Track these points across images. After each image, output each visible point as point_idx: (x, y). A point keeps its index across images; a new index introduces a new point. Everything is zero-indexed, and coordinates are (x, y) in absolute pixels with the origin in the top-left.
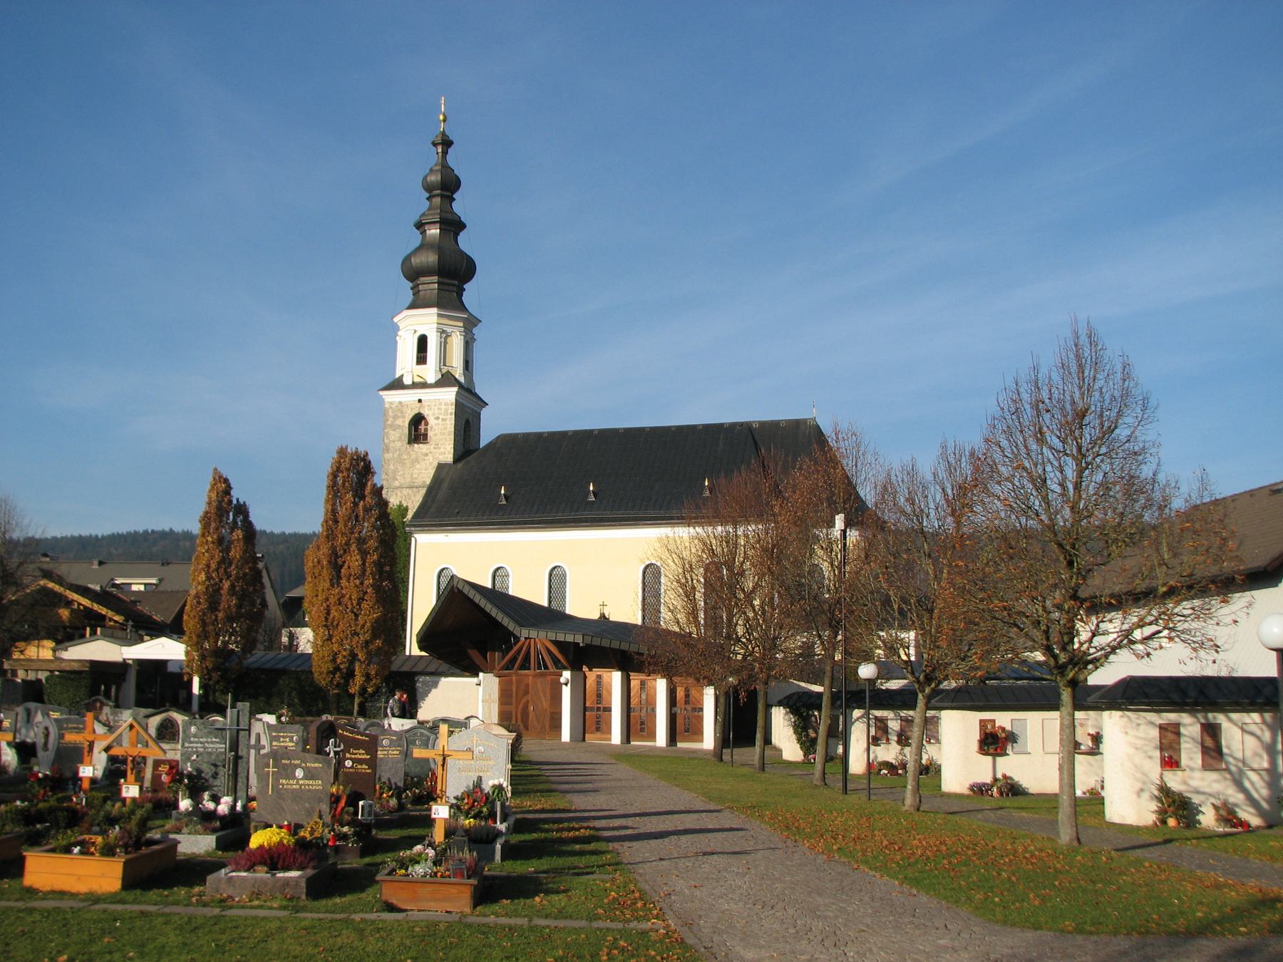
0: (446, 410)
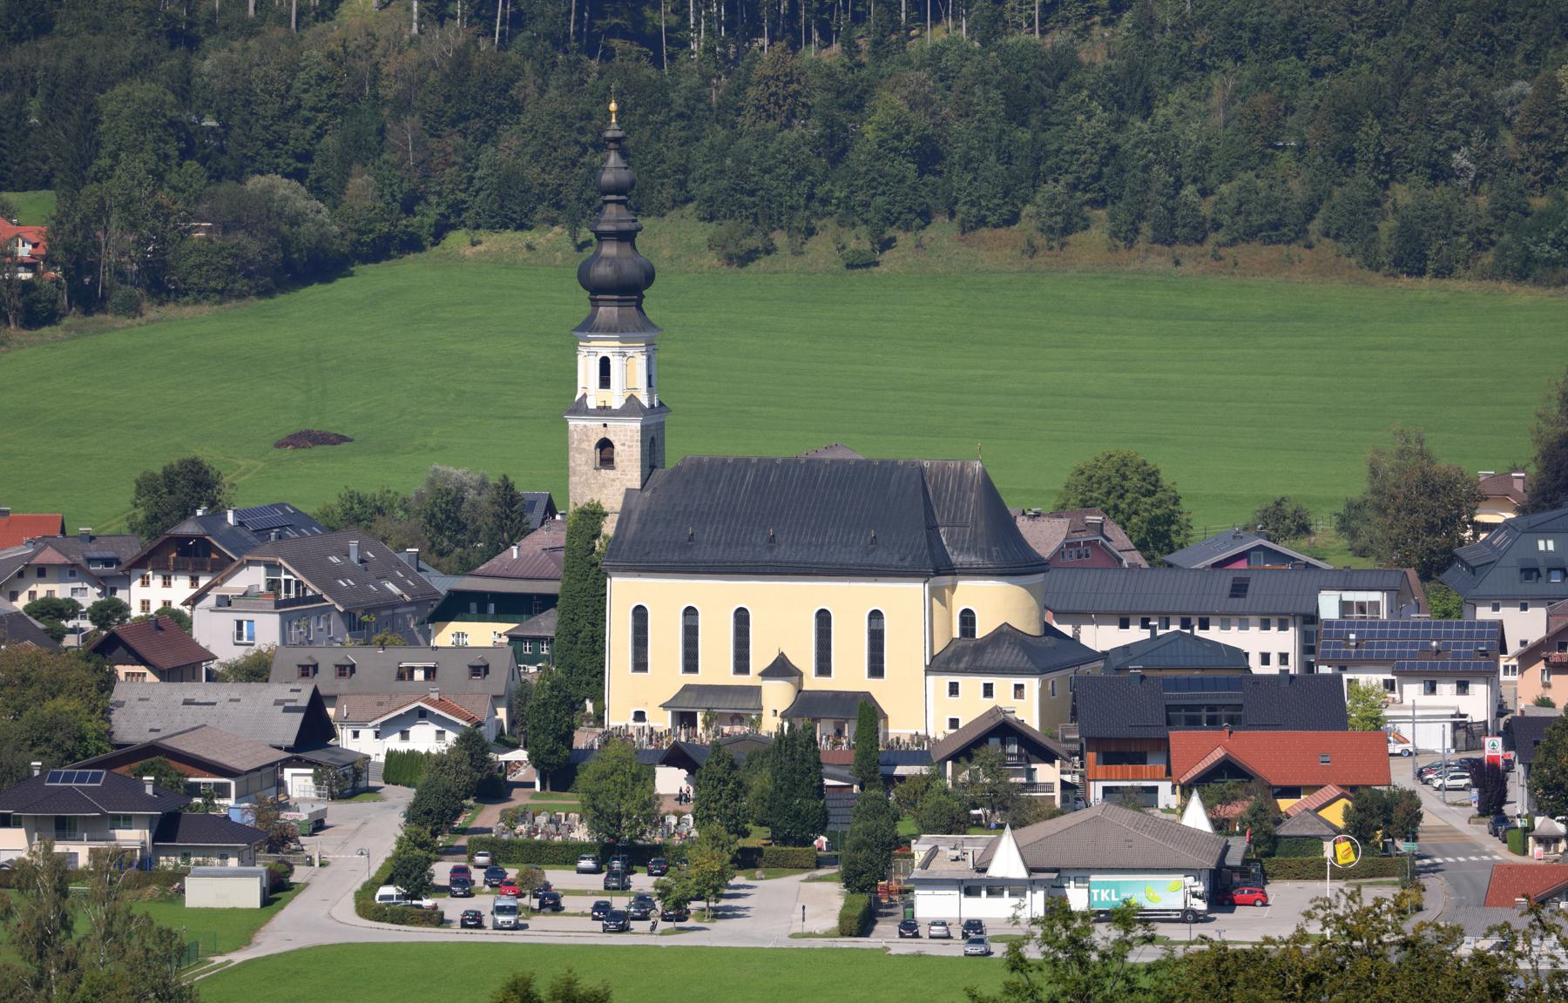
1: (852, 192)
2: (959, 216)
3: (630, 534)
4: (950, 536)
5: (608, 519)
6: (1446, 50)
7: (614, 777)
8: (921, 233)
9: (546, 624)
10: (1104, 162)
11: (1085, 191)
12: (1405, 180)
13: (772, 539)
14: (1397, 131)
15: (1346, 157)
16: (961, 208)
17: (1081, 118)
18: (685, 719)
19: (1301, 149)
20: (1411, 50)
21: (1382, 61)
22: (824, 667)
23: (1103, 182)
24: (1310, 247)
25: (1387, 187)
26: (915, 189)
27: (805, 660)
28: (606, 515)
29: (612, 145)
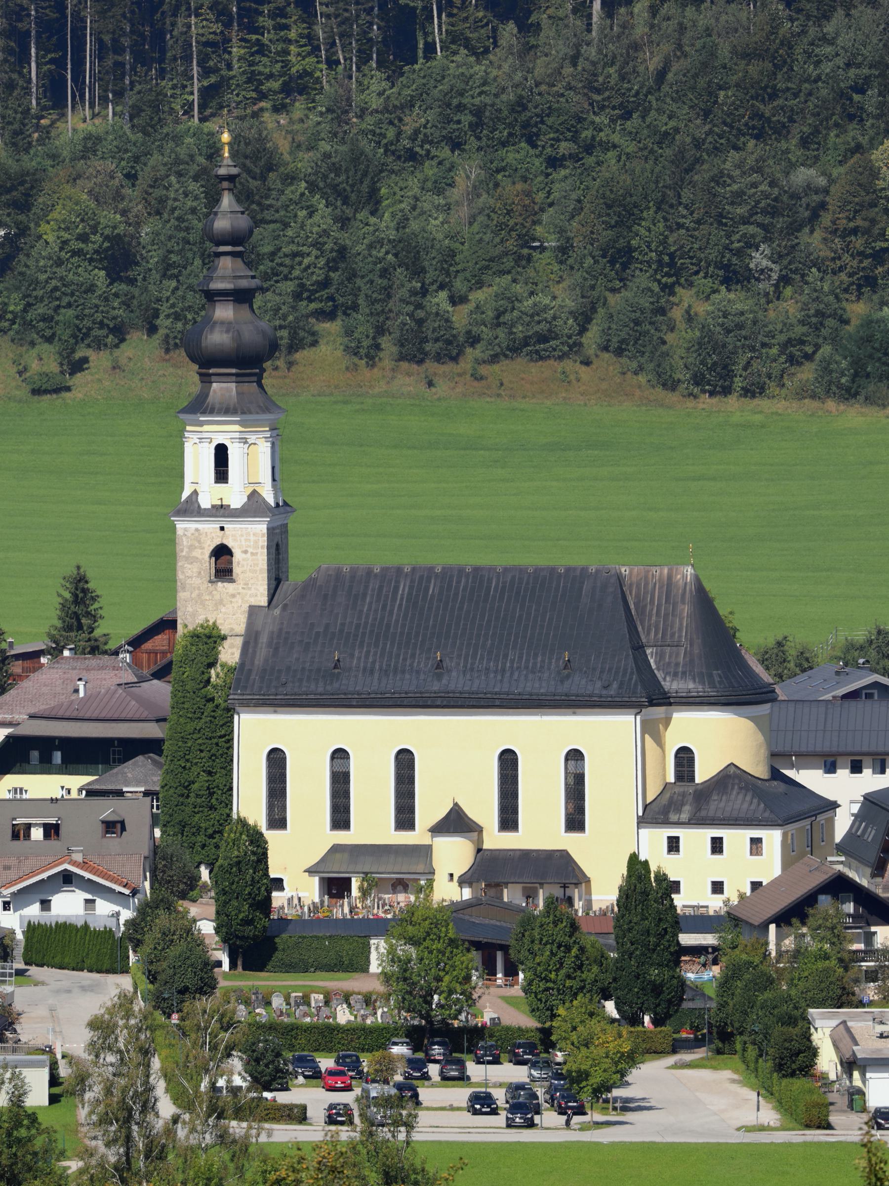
0: (256, 542)
1: (29, 305)
2: (162, 332)
3: (259, 661)
4: (660, 657)
5: (226, 644)
6: (707, 134)
7: (428, 943)
8: (117, 352)
9: (137, 778)
10: (332, 265)
11: (310, 300)
12: (691, 284)
13: (439, 665)
14: (680, 226)
15: (620, 258)
16: (163, 323)
17: (302, 214)
18: (336, 887)
19: (564, 250)
20: (666, 134)
21: (631, 148)
22: (509, 819)
23: (332, 290)
24: (587, 363)
25: (672, 293)
26: (106, 299)
27: (485, 810)
28: (224, 638)
29: (225, 184)
